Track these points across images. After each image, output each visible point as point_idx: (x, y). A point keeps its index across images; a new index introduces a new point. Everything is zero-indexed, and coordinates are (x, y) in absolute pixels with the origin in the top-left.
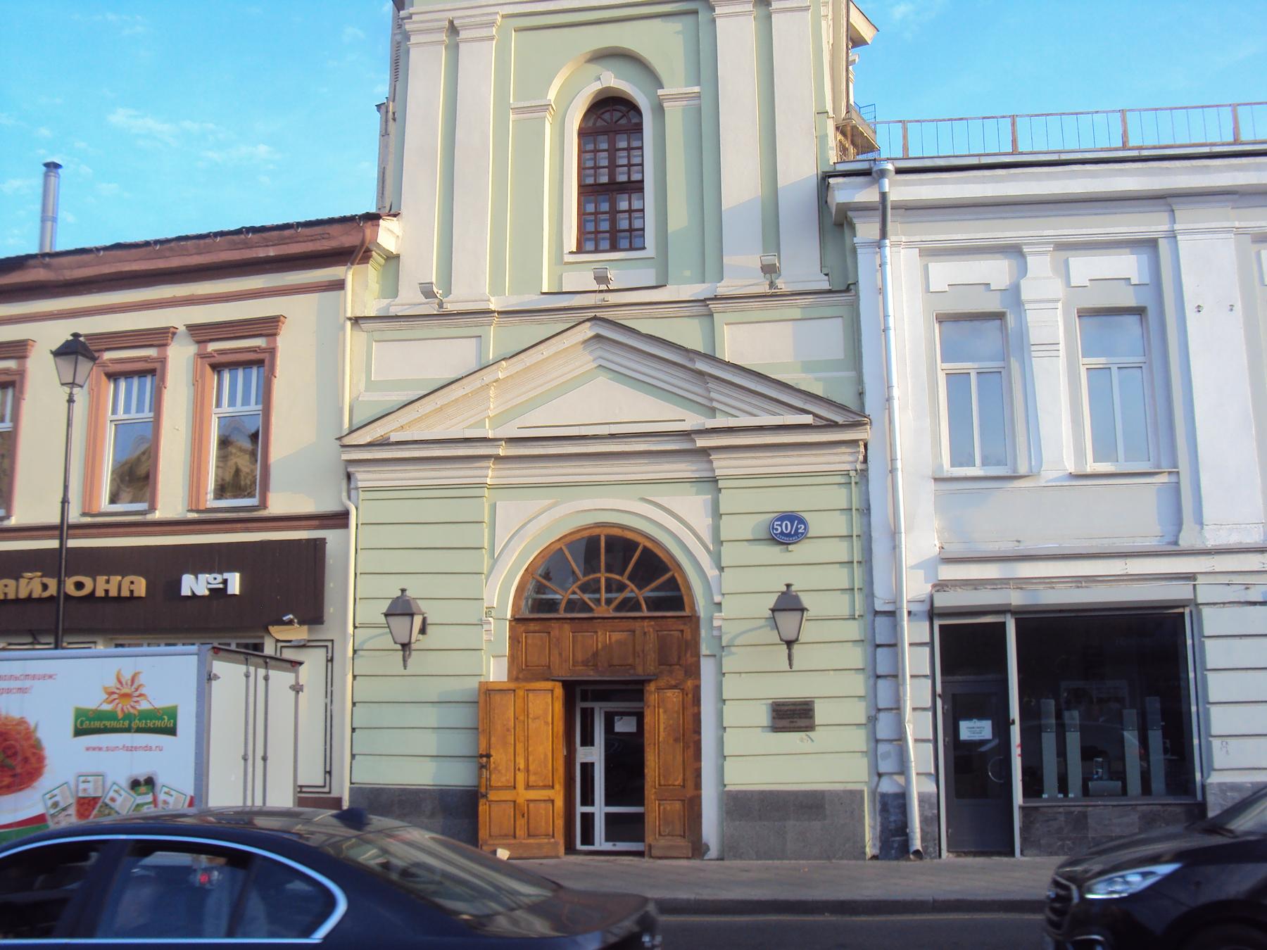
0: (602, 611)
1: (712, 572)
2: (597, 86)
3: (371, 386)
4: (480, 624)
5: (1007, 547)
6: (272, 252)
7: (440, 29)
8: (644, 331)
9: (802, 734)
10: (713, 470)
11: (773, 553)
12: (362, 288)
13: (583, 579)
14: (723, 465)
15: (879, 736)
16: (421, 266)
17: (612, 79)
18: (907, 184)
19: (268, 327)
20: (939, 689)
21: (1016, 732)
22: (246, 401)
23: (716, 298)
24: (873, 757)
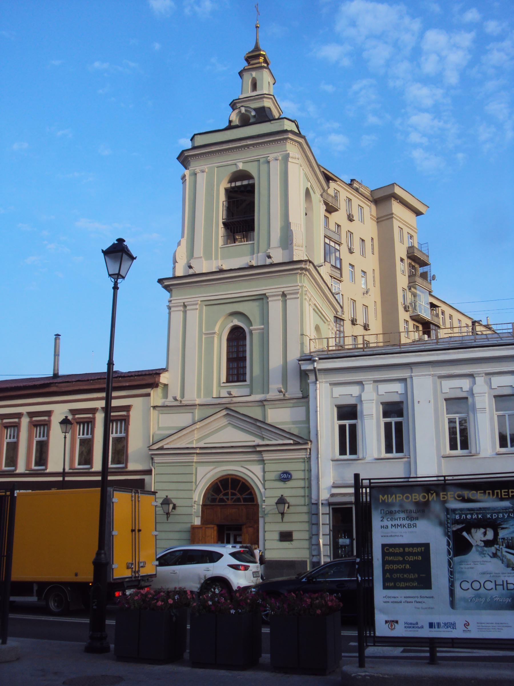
0: (229, 502)
1: (262, 490)
2: (232, 324)
3: (159, 428)
4: (192, 506)
6: (127, 384)
7: (181, 306)
8: (241, 413)
9: (289, 543)
10: (263, 457)
11: (281, 484)
12: (156, 396)
13: (224, 492)
14: (266, 456)
16: (175, 391)
17: (236, 322)
18: (323, 363)
19: (128, 408)
20: (331, 528)
21: (355, 542)
22: (121, 432)
23: (265, 400)
24: (310, 549)
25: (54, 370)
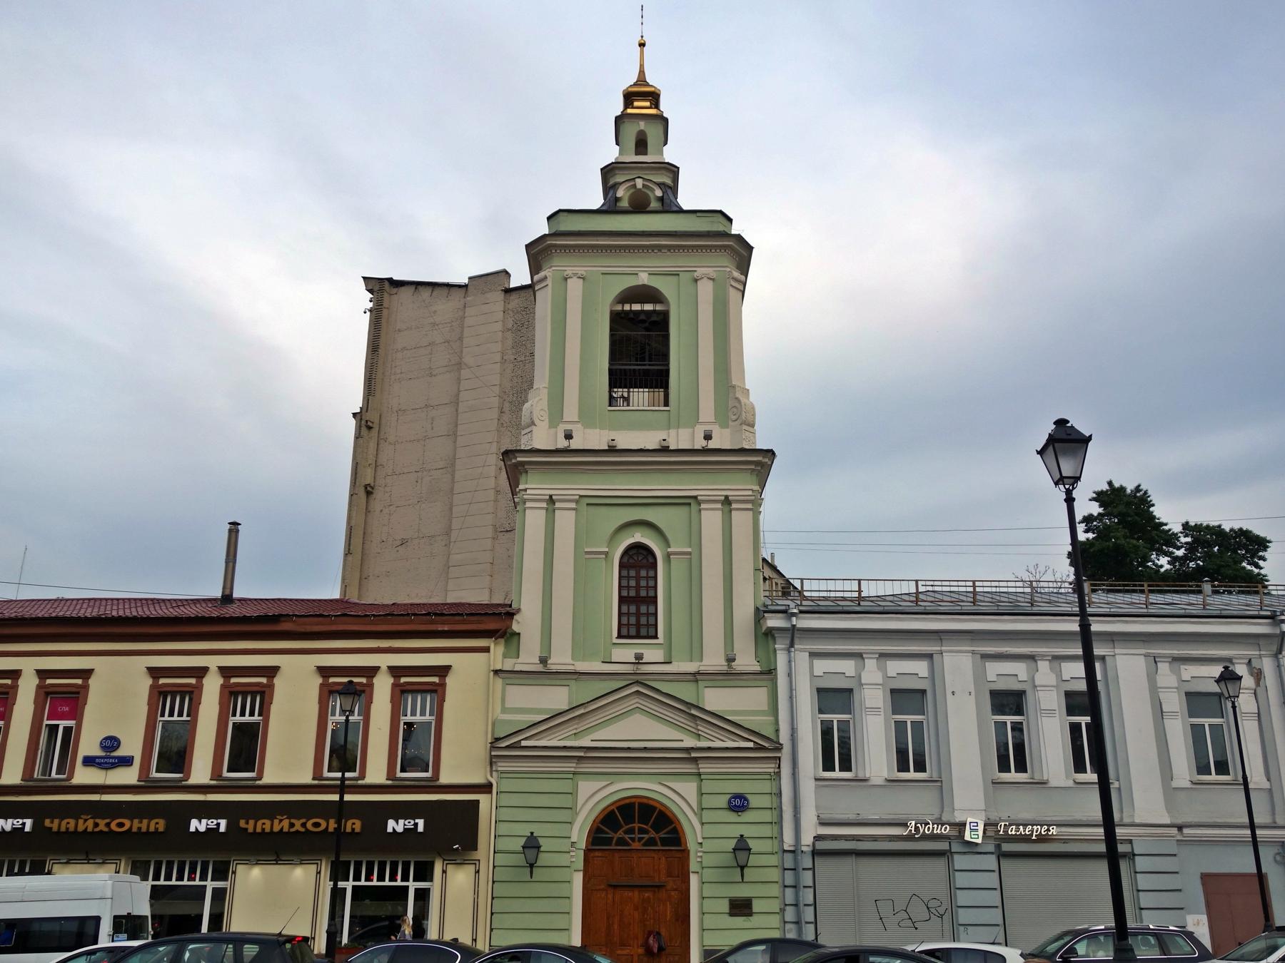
0: (636, 845)
5: (851, 817)
11: (732, 817)
14: (705, 768)
15: (787, 919)
25: (224, 588)
